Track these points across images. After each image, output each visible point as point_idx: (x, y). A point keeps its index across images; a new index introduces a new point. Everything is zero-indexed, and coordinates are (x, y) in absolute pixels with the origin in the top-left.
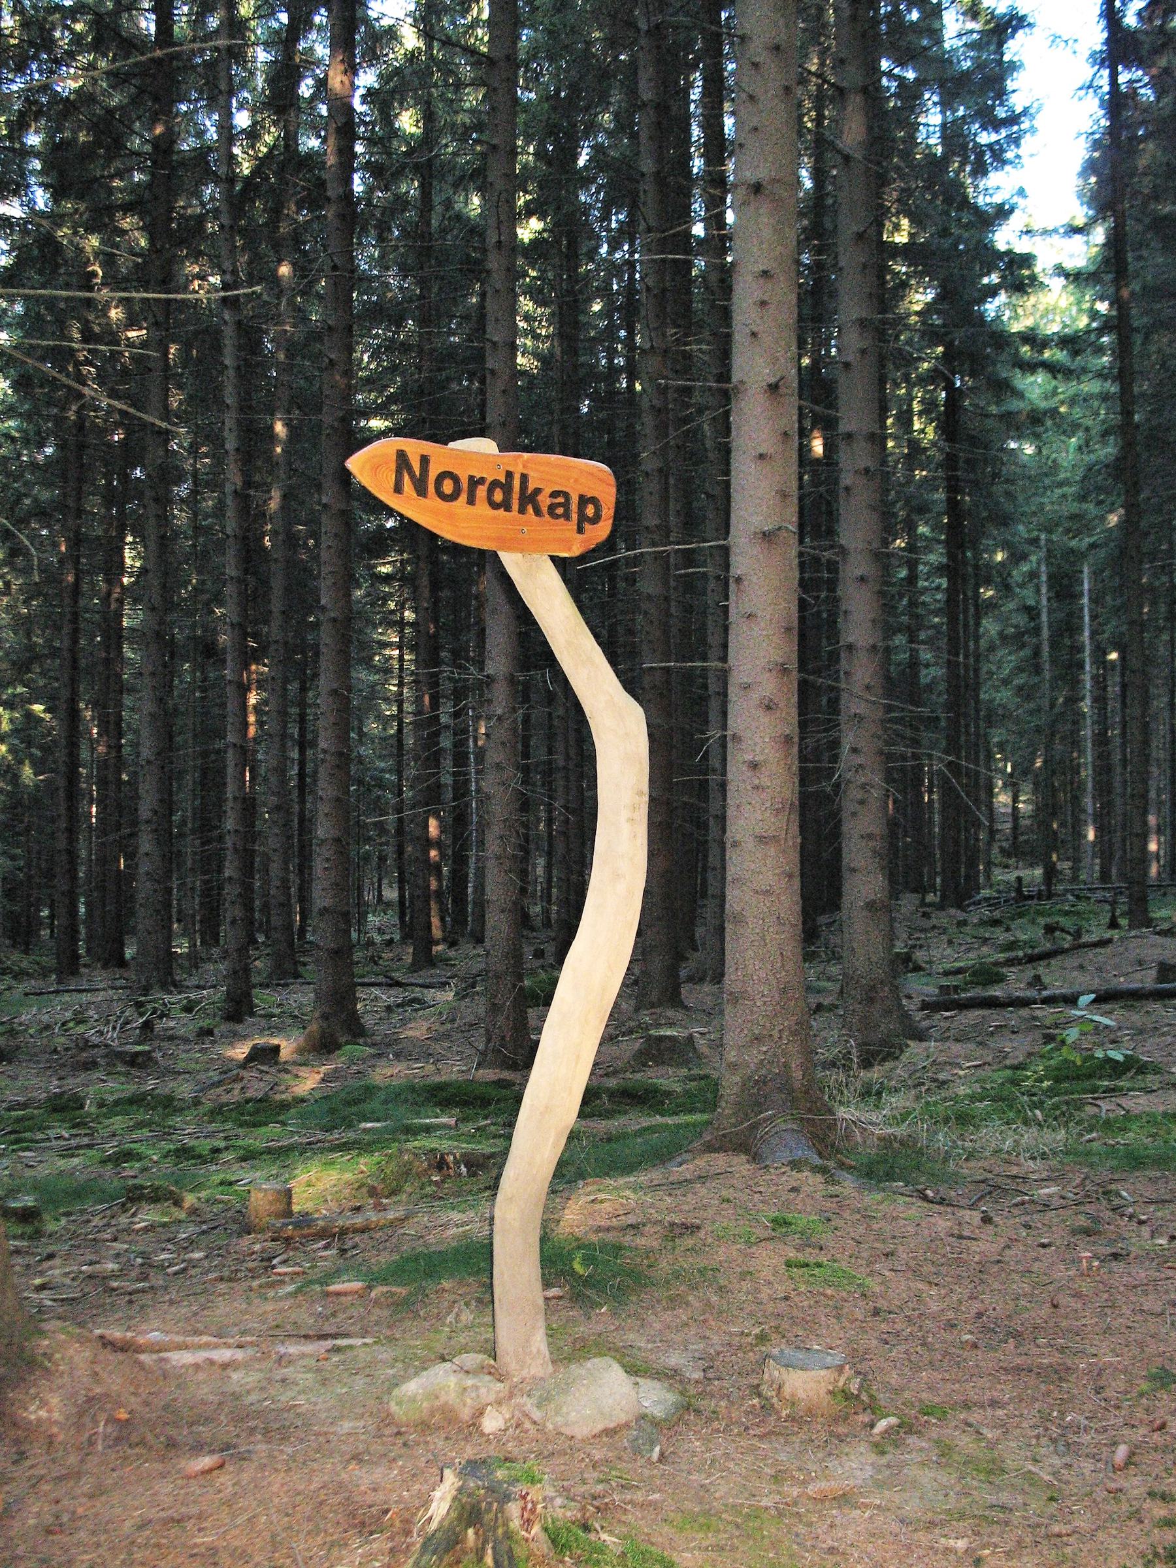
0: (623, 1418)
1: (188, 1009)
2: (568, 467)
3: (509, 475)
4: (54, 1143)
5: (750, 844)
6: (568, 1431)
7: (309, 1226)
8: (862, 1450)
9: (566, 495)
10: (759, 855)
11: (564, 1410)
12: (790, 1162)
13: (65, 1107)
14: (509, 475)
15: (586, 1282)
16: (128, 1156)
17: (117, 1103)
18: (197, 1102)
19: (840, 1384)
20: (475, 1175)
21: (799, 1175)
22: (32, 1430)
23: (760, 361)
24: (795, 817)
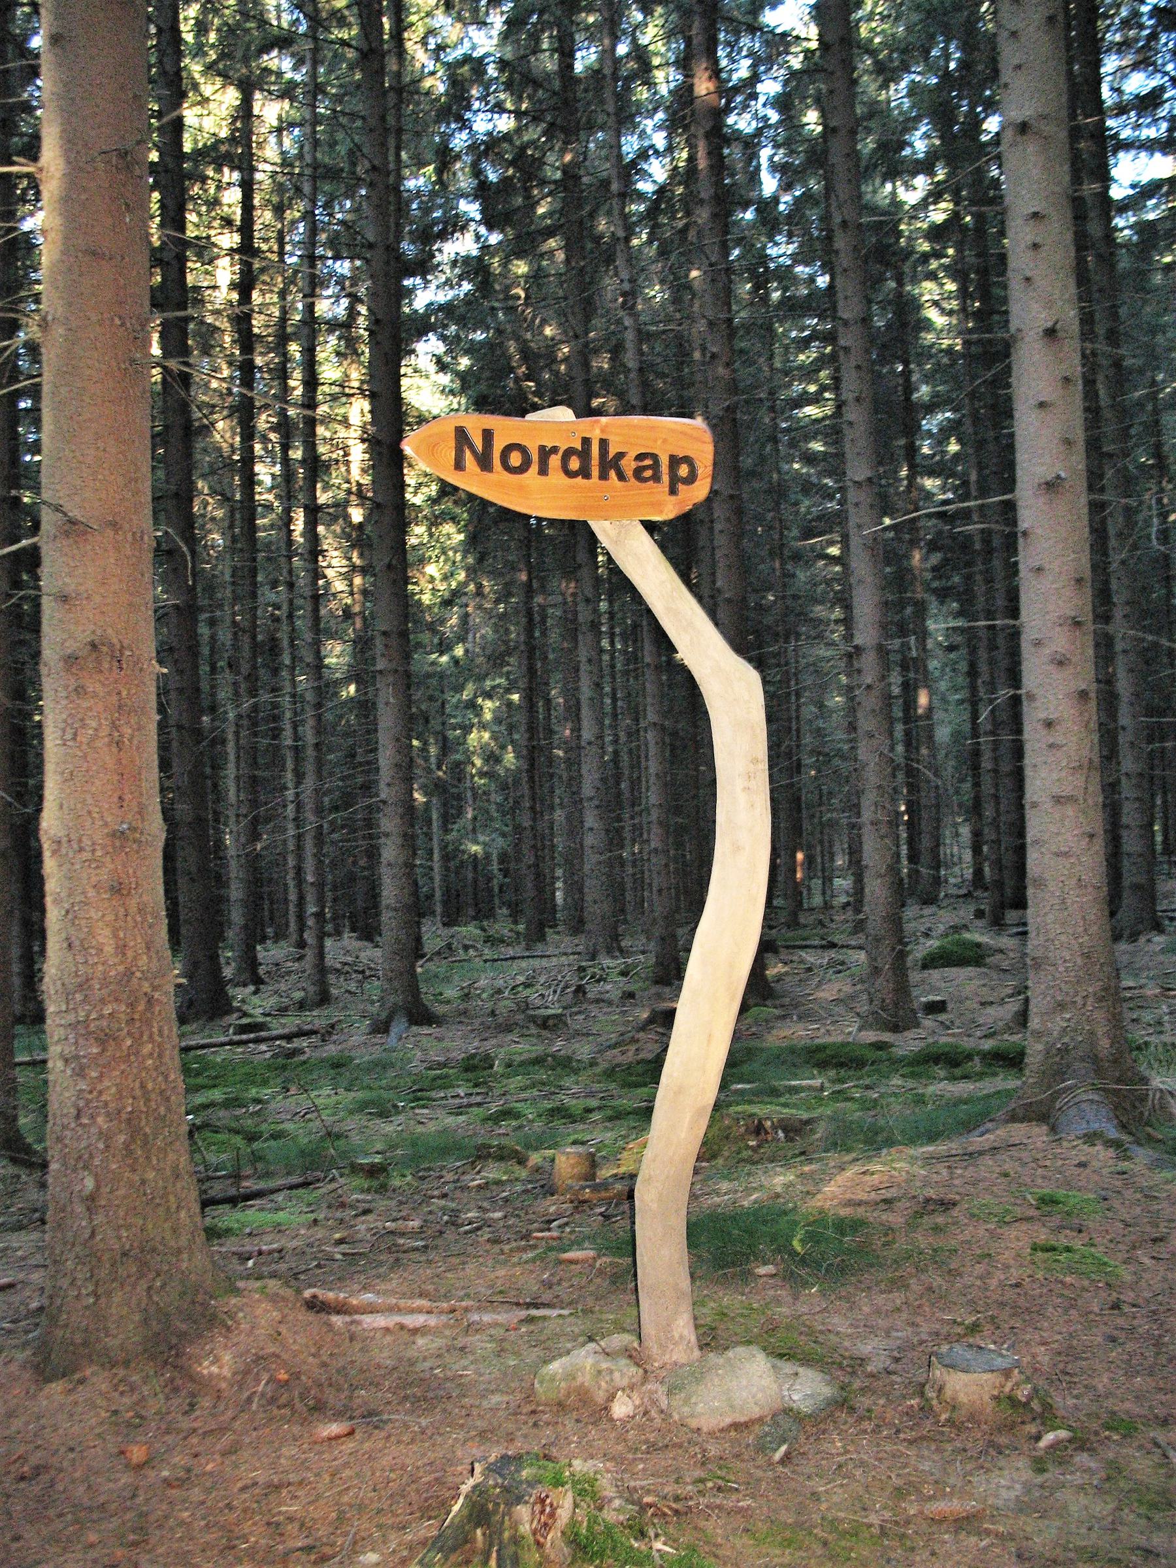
0: (756, 1412)
1: (624, 974)
2: (652, 428)
3: (586, 441)
4: (451, 1101)
5: (1048, 805)
6: (694, 1424)
7: (606, 1189)
8: (1020, 1465)
9: (655, 457)
10: (1057, 816)
11: (693, 1400)
12: (1085, 1135)
13: (476, 1067)
14: (586, 441)
15: (803, 1261)
16: (507, 1114)
17: (522, 1064)
18: (593, 1063)
19: (1007, 1389)
20: (792, 1140)
21: (1091, 1149)
22: (203, 1384)
23: (1035, 306)
24: (1096, 778)
